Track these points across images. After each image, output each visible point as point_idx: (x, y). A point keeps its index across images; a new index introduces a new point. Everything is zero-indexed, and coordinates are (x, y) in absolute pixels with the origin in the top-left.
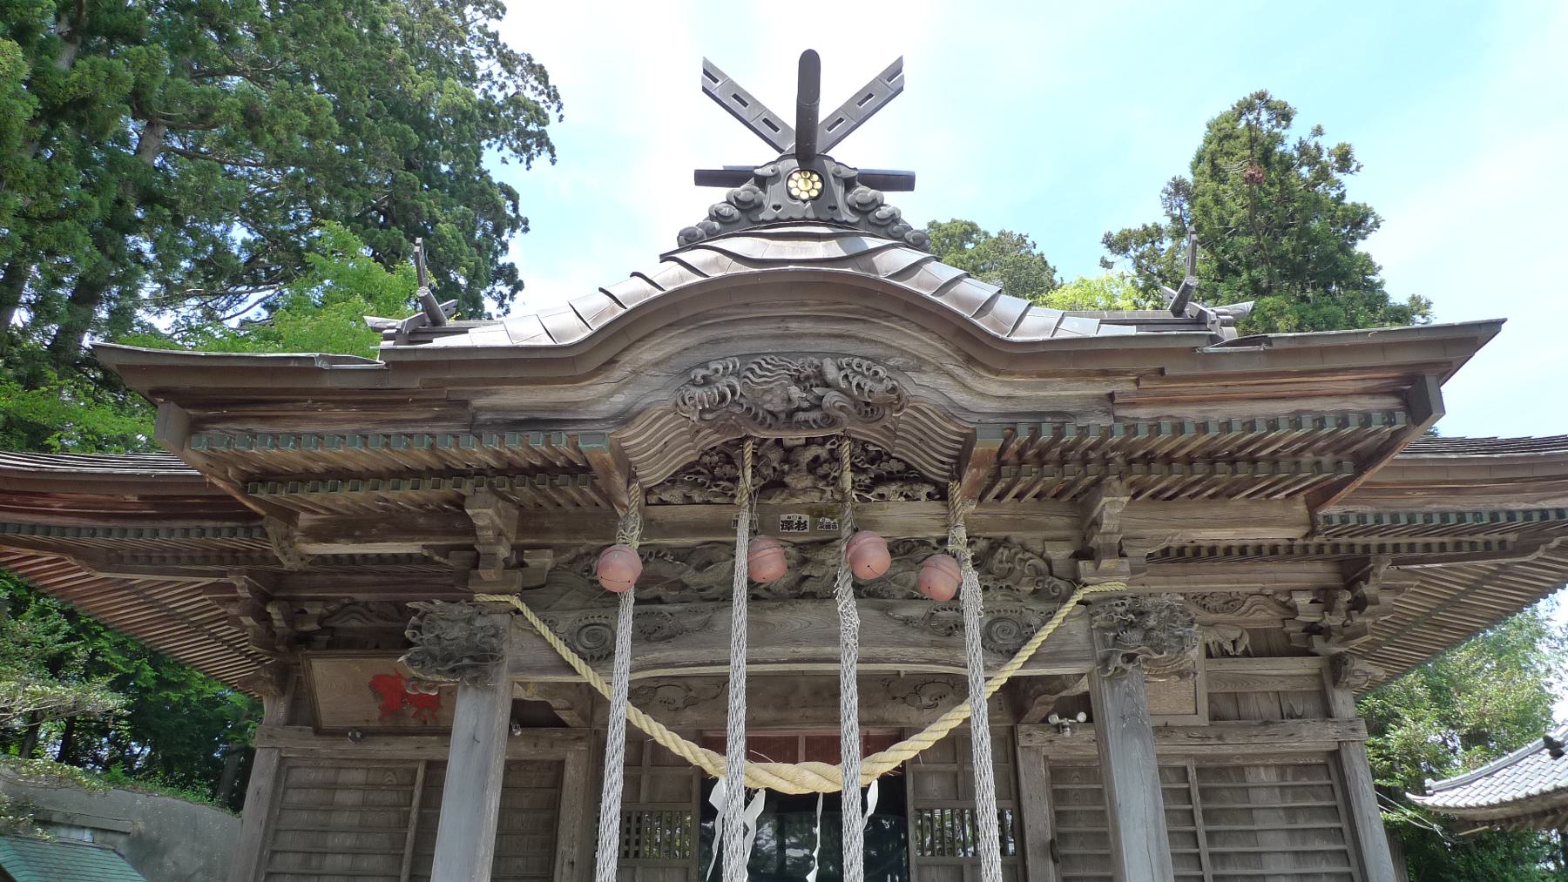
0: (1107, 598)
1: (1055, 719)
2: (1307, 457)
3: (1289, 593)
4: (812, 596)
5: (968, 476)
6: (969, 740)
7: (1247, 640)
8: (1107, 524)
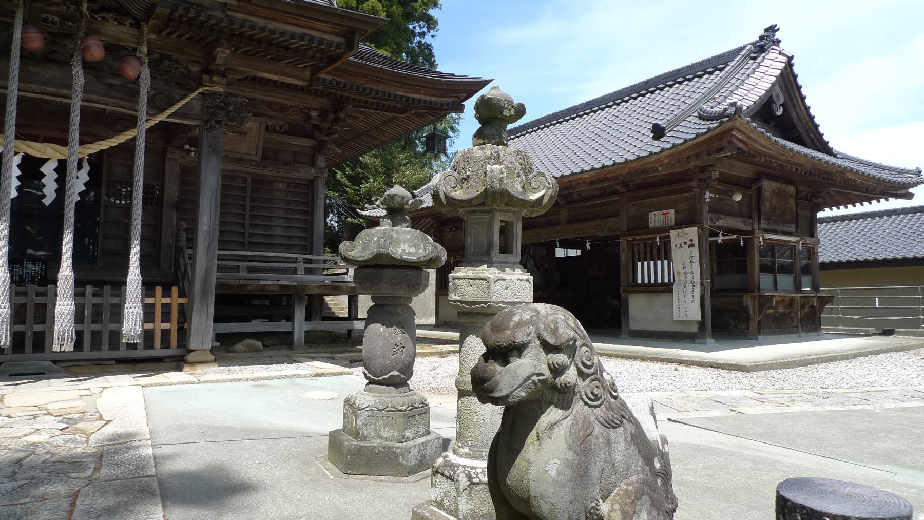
0: (214, 94)
1: (187, 147)
2: (310, 53)
3: (309, 109)
4: (57, 62)
5: (151, 22)
6: (134, 146)
7: (287, 127)
8: (219, 60)
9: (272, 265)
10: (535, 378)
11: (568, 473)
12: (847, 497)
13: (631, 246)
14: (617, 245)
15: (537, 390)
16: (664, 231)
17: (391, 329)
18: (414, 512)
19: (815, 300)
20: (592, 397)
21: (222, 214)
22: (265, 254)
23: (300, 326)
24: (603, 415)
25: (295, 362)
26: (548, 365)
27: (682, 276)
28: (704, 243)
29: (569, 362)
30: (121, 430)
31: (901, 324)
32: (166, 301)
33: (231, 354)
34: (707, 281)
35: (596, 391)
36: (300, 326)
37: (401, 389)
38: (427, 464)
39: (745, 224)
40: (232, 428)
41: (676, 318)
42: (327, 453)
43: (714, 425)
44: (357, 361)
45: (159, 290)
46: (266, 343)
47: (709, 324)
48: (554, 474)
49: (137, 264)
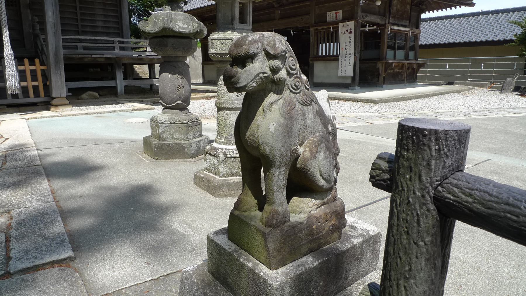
9: (98, 45)
10: (261, 75)
11: (281, 130)
12: (436, 124)
13: (316, 33)
14: (308, 33)
15: (263, 83)
16: (335, 23)
17: (175, 76)
18: (195, 175)
19: (415, 65)
20: (295, 88)
21: (61, 12)
22: (93, 38)
23: (120, 83)
24: (301, 98)
25: (120, 103)
26: (270, 67)
27: (344, 51)
28: (358, 31)
29: (282, 66)
30: (16, 143)
31: (458, 79)
32: (33, 68)
33: (79, 101)
34: (358, 53)
35: (297, 84)
36: (120, 83)
37: (183, 111)
38: (201, 152)
39: (381, 20)
40: (85, 139)
41: (340, 75)
42: (143, 149)
43: (357, 130)
44: (157, 103)
45: (26, 61)
46: (100, 94)
47: (357, 78)
48: (273, 130)
49: (10, 48)
